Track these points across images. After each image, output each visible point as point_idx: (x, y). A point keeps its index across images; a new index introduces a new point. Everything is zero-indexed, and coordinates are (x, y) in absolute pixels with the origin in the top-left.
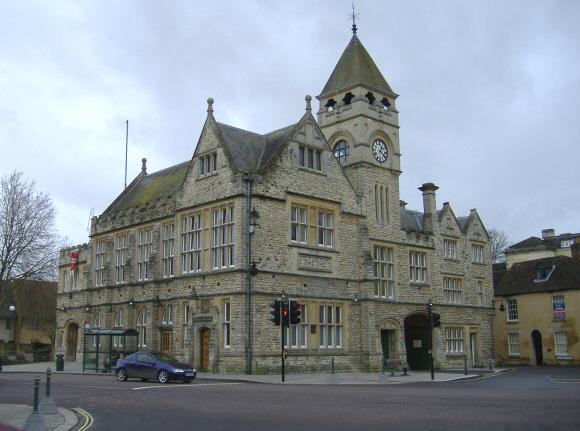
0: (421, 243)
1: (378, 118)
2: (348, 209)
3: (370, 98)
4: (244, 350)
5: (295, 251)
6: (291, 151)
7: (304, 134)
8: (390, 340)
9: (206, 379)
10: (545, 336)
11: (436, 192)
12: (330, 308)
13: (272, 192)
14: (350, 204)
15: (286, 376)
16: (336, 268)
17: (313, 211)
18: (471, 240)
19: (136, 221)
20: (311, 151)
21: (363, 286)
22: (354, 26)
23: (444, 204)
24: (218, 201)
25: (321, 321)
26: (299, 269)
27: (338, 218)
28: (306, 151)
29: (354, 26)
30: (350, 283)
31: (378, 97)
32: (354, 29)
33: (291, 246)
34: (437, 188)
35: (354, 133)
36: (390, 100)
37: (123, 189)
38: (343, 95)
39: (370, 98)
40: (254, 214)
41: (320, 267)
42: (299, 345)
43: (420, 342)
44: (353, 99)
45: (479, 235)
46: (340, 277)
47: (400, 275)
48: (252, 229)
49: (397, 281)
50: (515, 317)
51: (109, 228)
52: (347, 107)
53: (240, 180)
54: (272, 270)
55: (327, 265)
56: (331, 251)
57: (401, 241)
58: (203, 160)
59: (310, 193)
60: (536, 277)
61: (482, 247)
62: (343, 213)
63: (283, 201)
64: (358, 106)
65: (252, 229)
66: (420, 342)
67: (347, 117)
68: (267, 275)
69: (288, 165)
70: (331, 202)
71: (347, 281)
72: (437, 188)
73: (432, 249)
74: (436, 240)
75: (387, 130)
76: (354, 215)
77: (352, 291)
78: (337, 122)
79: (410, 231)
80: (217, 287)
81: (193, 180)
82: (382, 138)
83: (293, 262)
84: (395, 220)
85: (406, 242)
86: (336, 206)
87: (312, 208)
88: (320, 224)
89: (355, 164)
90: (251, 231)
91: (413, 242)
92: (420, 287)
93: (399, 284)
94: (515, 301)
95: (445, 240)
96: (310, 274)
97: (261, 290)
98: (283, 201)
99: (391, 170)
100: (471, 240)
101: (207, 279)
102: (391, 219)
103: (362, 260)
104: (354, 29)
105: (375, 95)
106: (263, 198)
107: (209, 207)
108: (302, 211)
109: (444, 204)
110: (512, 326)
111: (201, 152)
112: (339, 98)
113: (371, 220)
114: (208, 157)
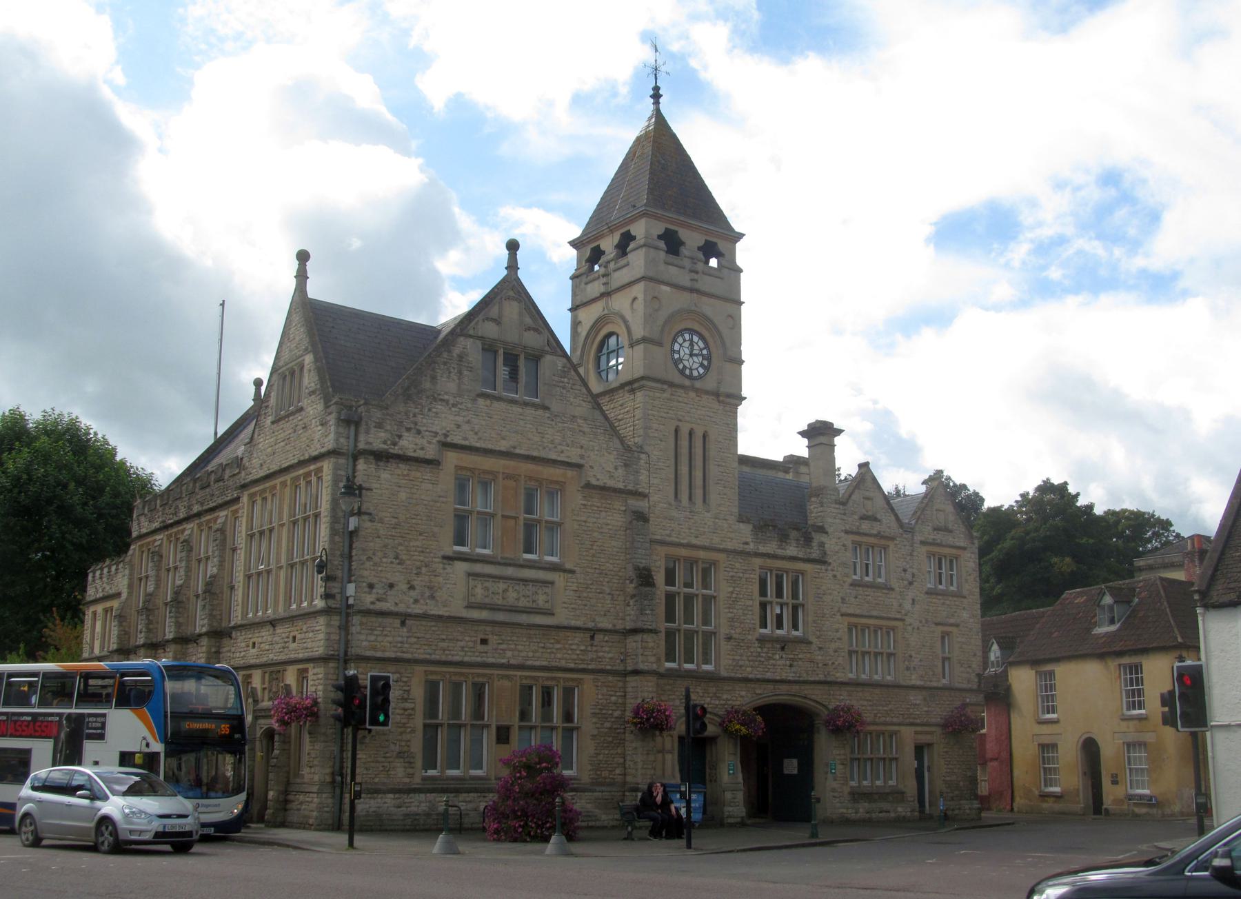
0: (792, 550)
1: (688, 284)
2: (598, 476)
3: (672, 243)
4: (328, 779)
5: (461, 567)
6: (461, 357)
7: (497, 322)
8: (708, 758)
9: (592, 827)
10: (1109, 751)
11: (837, 440)
12: (457, 687)
13: (408, 444)
14: (604, 466)
15: (356, 838)
16: (565, 602)
17: (511, 483)
18: (923, 543)
19: (196, 509)
20: (511, 360)
21: (633, 643)
22: (656, 89)
23: (860, 466)
24: (301, 463)
25: (524, 715)
26: (470, 606)
27: (576, 498)
28: (521, 363)
29: (656, 89)
30: (599, 637)
31: (692, 239)
32: (656, 96)
33: (449, 559)
34: (839, 432)
35: (628, 317)
36: (722, 245)
37: (212, 441)
38: (616, 238)
39: (672, 243)
40: (352, 489)
41: (523, 603)
42: (442, 771)
43: (795, 762)
44: (632, 245)
45: (947, 530)
46: (573, 623)
47: (732, 620)
48: (353, 523)
49: (724, 630)
50: (1052, 710)
51: (156, 525)
52: (623, 262)
53: (332, 420)
54: (401, 608)
55: (479, 591)
56: (555, 568)
57: (740, 547)
58: (284, 378)
59: (503, 446)
60: (1095, 625)
61: (885, 548)
62: (588, 486)
63: (433, 463)
64: (637, 261)
65: (353, 523)
66: (795, 762)
67: (626, 280)
68: (388, 620)
69: (452, 386)
70: (554, 462)
71: (593, 632)
72: (839, 432)
73: (822, 561)
74: (831, 544)
75: (708, 307)
76: (615, 490)
77: (608, 654)
78: (603, 295)
79: (762, 528)
80: (292, 646)
81: (269, 420)
82: (696, 327)
83: (454, 590)
84: (724, 500)
85: (752, 546)
86: (570, 473)
87: (508, 477)
88: (529, 510)
89: (630, 383)
90: (351, 528)
91: (771, 547)
92: (784, 644)
93: (729, 638)
94: (1051, 674)
95: (857, 545)
96: (500, 617)
97: (369, 653)
98: (433, 463)
99: (717, 395)
100: (923, 543)
101: (279, 630)
102: (714, 498)
103: (630, 588)
104: (656, 96)
105: (683, 234)
106: (381, 457)
107: (288, 478)
108: (485, 485)
109: (860, 466)
110: (1045, 729)
111: (281, 364)
112: (608, 245)
113: (659, 498)
114: (292, 373)
